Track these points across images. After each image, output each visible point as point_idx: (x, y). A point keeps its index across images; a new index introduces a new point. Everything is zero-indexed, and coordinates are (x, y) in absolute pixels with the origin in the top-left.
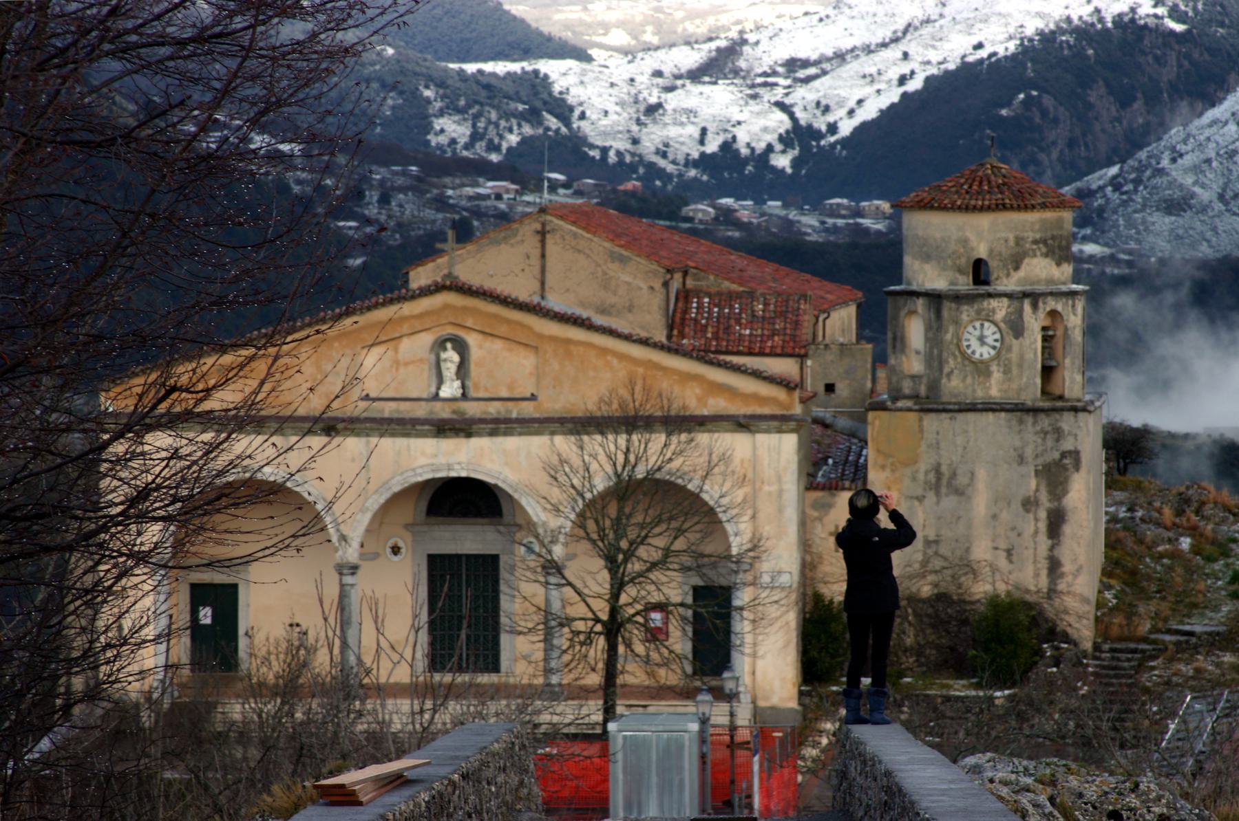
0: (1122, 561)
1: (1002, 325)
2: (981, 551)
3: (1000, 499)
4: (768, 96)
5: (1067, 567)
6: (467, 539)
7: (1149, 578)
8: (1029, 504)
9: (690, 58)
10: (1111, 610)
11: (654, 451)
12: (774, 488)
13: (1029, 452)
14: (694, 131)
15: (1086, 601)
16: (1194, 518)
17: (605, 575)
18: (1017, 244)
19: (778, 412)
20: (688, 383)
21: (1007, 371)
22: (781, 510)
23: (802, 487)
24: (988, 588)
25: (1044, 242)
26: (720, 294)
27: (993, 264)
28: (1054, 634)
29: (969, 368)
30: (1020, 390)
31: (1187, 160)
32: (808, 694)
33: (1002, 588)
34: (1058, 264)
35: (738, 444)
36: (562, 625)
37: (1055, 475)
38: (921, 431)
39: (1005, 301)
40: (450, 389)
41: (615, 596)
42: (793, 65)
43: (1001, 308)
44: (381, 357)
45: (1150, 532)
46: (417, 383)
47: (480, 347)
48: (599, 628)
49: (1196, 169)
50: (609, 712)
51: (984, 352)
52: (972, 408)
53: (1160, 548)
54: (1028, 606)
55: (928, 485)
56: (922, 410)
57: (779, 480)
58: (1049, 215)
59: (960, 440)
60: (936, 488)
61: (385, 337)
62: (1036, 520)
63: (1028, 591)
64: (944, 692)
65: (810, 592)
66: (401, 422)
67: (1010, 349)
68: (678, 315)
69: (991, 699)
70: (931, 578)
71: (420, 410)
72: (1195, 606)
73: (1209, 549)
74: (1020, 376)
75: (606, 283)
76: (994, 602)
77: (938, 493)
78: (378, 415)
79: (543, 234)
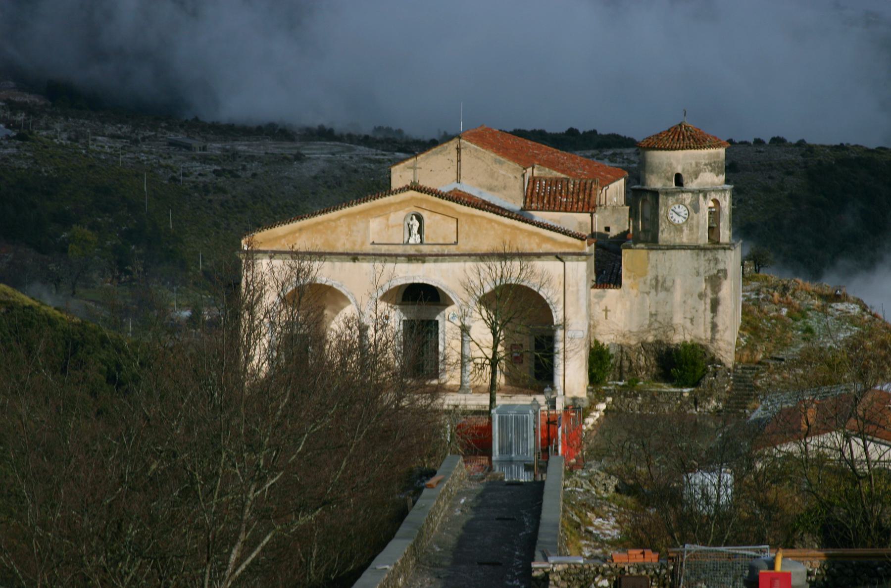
0: (751, 325)
1: (689, 207)
2: (678, 319)
3: (687, 293)
5: (721, 327)
7: (763, 330)
8: (701, 296)
10: (743, 348)
11: (514, 271)
12: (575, 289)
13: (702, 270)
15: (729, 344)
16: (790, 297)
17: (490, 337)
18: (697, 166)
19: (577, 251)
20: (526, 237)
21: (691, 229)
22: (578, 300)
23: (589, 287)
24: (682, 337)
25: (710, 164)
26: (551, 179)
27: (684, 176)
28: (713, 360)
29: (672, 228)
30: (697, 239)
32: (592, 390)
33: (688, 338)
34: (717, 175)
36: (470, 361)
37: (715, 281)
38: (649, 259)
39: (690, 194)
40: (415, 239)
41: (495, 347)
43: (688, 198)
45: (766, 308)
46: (398, 236)
47: (429, 218)
48: (487, 362)
50: (492, 400)
51: (679, 220)
52: (673, 248)
53: (771, 315)
54: (702, 346)
55: (652, 287)
56: (649, 249)
57: (577, 284)
58: (712, 151)
59: (667, 264)
60: (656, 287)
61: (383, 211)
62: (705, 304)
63: (701, 339)
64: (659, 389)
65: (593, 340)
66: (390, 255)
67: (692, 218)
68: (530, 191)
69: (682, 393)
70: (653, 332)
71: (399, 250)
72: (786, 345)
73: (796, 314)
74: (698, 232)
75: (492, 175)
76: (685, 345)
77: (656, 290)
78: (378, 252)
79: (459, 150)
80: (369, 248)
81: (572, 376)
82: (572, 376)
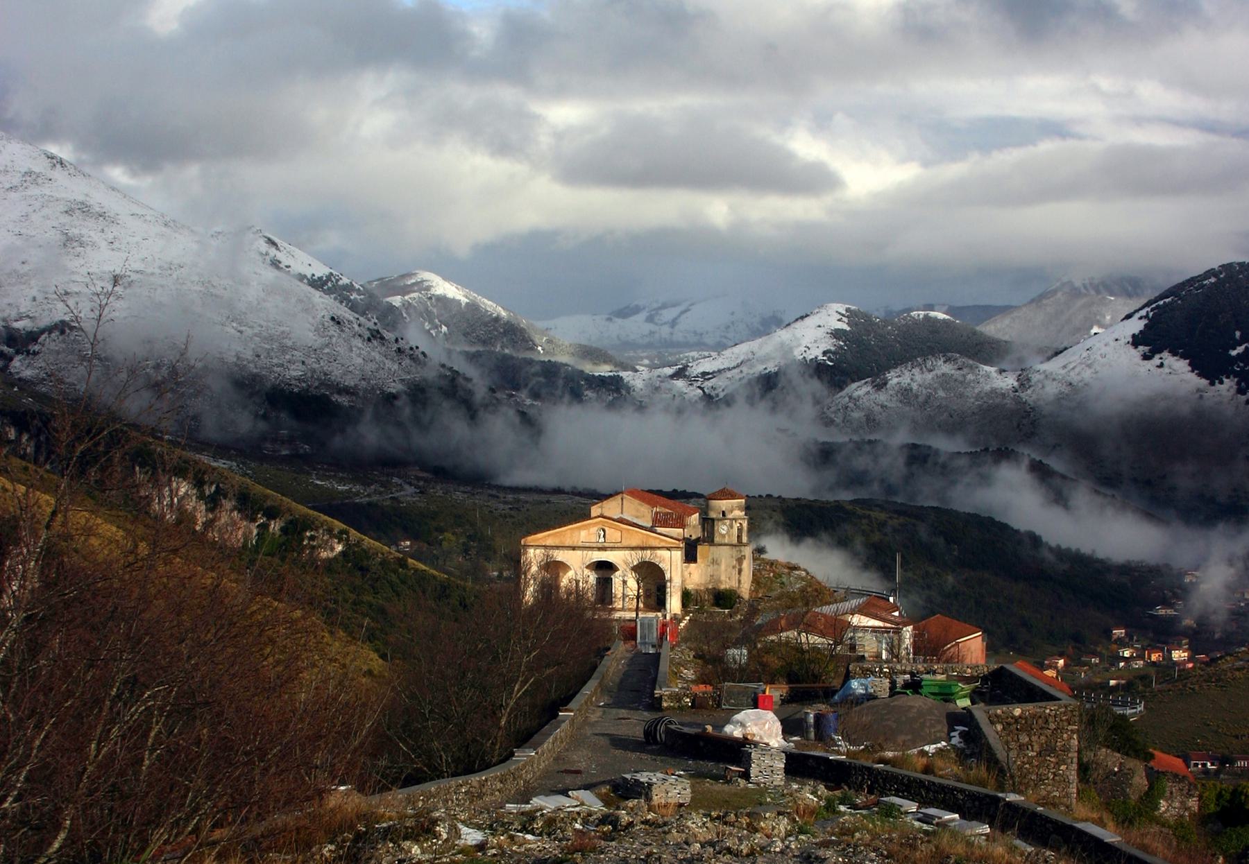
0: (756, 580)
2: (723, 578)
3: (727, 566)
4: (696, 384)
6: (605, 574)
9: (669, 371)
11: (647, 555)
14: (669, 396)
20: (653, 539)
31: (833, 409)
35: (666, 553)
37: (740, 560)
40: (602, 540)
42: (704, 374)
43: (728, 522)
44: (584, 533)
49: (835, 412)
80: (580, 544)
81: (674, 604)
82: (674, 604)
